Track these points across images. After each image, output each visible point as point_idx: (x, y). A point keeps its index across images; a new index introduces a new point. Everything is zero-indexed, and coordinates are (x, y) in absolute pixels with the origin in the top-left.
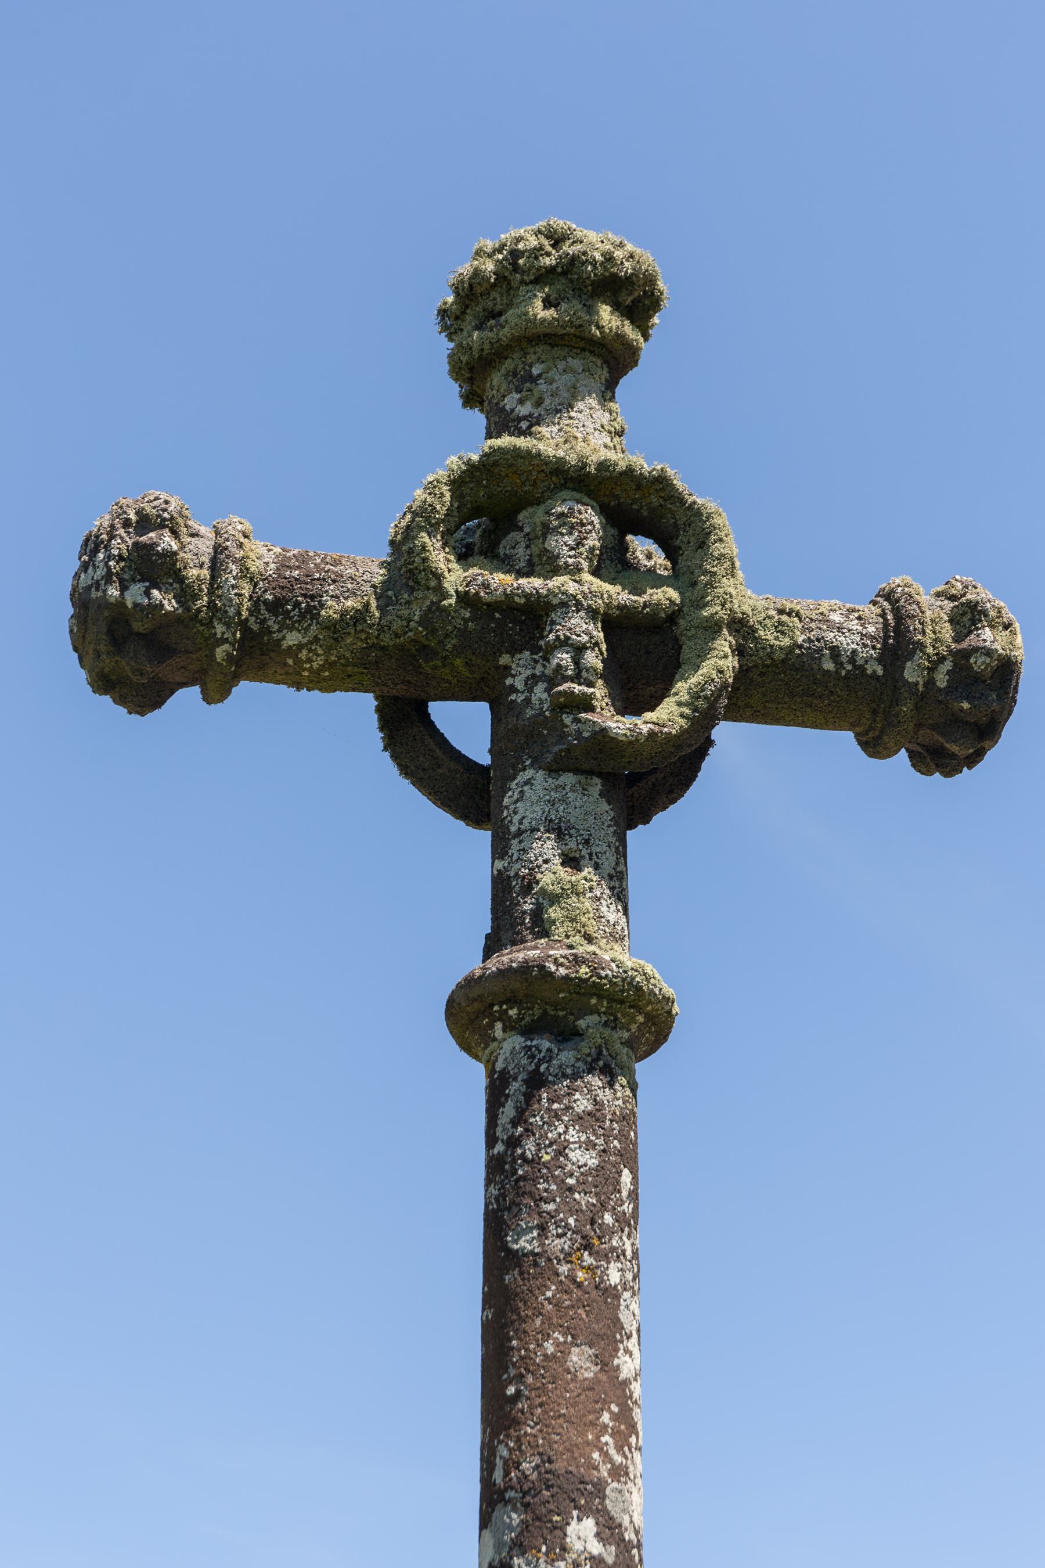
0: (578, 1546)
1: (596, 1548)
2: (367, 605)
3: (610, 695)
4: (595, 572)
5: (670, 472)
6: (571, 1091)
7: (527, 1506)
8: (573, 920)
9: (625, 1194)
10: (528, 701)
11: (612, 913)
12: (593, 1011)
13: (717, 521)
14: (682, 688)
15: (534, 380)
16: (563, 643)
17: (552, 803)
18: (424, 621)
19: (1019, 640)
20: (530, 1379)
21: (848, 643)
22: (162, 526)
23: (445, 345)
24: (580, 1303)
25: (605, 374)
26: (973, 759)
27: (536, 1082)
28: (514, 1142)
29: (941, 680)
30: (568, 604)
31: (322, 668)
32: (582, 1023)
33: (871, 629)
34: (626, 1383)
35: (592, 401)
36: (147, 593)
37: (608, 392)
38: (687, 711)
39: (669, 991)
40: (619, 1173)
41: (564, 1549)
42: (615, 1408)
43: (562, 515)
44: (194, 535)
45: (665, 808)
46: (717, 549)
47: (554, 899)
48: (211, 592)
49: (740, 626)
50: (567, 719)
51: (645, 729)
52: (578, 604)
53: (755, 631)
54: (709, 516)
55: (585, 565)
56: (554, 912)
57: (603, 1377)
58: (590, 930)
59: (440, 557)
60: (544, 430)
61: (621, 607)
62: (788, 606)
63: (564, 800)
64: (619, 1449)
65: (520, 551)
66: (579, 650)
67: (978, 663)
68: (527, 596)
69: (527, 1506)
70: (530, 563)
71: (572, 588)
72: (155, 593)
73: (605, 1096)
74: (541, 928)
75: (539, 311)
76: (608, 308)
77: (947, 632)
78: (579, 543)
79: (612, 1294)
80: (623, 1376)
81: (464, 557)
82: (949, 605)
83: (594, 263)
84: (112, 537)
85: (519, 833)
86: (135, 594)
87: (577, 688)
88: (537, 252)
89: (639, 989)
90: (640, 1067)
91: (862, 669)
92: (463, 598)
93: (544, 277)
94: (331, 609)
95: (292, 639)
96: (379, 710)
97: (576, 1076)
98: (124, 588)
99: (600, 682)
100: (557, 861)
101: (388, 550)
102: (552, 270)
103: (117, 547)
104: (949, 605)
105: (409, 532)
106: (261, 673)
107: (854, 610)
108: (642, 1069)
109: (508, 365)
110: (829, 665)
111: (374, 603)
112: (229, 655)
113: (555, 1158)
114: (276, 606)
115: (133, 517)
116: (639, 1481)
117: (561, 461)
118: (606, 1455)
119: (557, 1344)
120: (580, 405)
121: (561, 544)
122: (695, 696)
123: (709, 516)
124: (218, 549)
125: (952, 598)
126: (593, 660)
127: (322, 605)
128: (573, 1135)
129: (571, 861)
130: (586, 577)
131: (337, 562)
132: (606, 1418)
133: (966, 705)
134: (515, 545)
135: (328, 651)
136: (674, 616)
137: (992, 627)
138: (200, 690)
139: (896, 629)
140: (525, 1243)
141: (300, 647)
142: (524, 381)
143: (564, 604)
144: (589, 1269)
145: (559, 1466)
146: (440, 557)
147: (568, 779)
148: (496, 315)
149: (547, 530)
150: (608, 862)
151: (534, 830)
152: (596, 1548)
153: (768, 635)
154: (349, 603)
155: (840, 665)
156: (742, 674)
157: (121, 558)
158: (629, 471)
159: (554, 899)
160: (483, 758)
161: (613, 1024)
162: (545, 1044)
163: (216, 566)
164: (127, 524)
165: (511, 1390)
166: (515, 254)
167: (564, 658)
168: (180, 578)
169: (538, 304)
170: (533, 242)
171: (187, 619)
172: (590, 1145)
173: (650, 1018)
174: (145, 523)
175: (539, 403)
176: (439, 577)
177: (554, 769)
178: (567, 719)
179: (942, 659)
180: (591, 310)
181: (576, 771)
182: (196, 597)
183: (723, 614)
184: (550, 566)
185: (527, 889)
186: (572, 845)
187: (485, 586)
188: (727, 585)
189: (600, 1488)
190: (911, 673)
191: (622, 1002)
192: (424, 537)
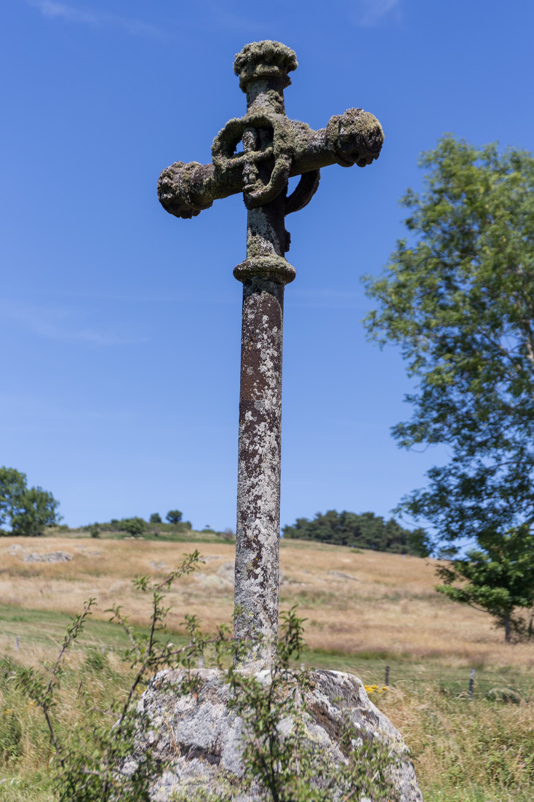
4: (256, 150)
12: (254, 276)
21: (317, 143)
24: (249, 356)
42: (258, 381)
52: (247, 163)
78: (247, 144)
79: (259, 350)
91: (322, 149)
110: (315, 152)
118: (255, 394)
120: (258, 97)
138: (336, 167)
141: (205, 193)
144: (252, 346)
152: (251, 418)
156: (292, 165)
172: (253, 313)
181: (255, 207)
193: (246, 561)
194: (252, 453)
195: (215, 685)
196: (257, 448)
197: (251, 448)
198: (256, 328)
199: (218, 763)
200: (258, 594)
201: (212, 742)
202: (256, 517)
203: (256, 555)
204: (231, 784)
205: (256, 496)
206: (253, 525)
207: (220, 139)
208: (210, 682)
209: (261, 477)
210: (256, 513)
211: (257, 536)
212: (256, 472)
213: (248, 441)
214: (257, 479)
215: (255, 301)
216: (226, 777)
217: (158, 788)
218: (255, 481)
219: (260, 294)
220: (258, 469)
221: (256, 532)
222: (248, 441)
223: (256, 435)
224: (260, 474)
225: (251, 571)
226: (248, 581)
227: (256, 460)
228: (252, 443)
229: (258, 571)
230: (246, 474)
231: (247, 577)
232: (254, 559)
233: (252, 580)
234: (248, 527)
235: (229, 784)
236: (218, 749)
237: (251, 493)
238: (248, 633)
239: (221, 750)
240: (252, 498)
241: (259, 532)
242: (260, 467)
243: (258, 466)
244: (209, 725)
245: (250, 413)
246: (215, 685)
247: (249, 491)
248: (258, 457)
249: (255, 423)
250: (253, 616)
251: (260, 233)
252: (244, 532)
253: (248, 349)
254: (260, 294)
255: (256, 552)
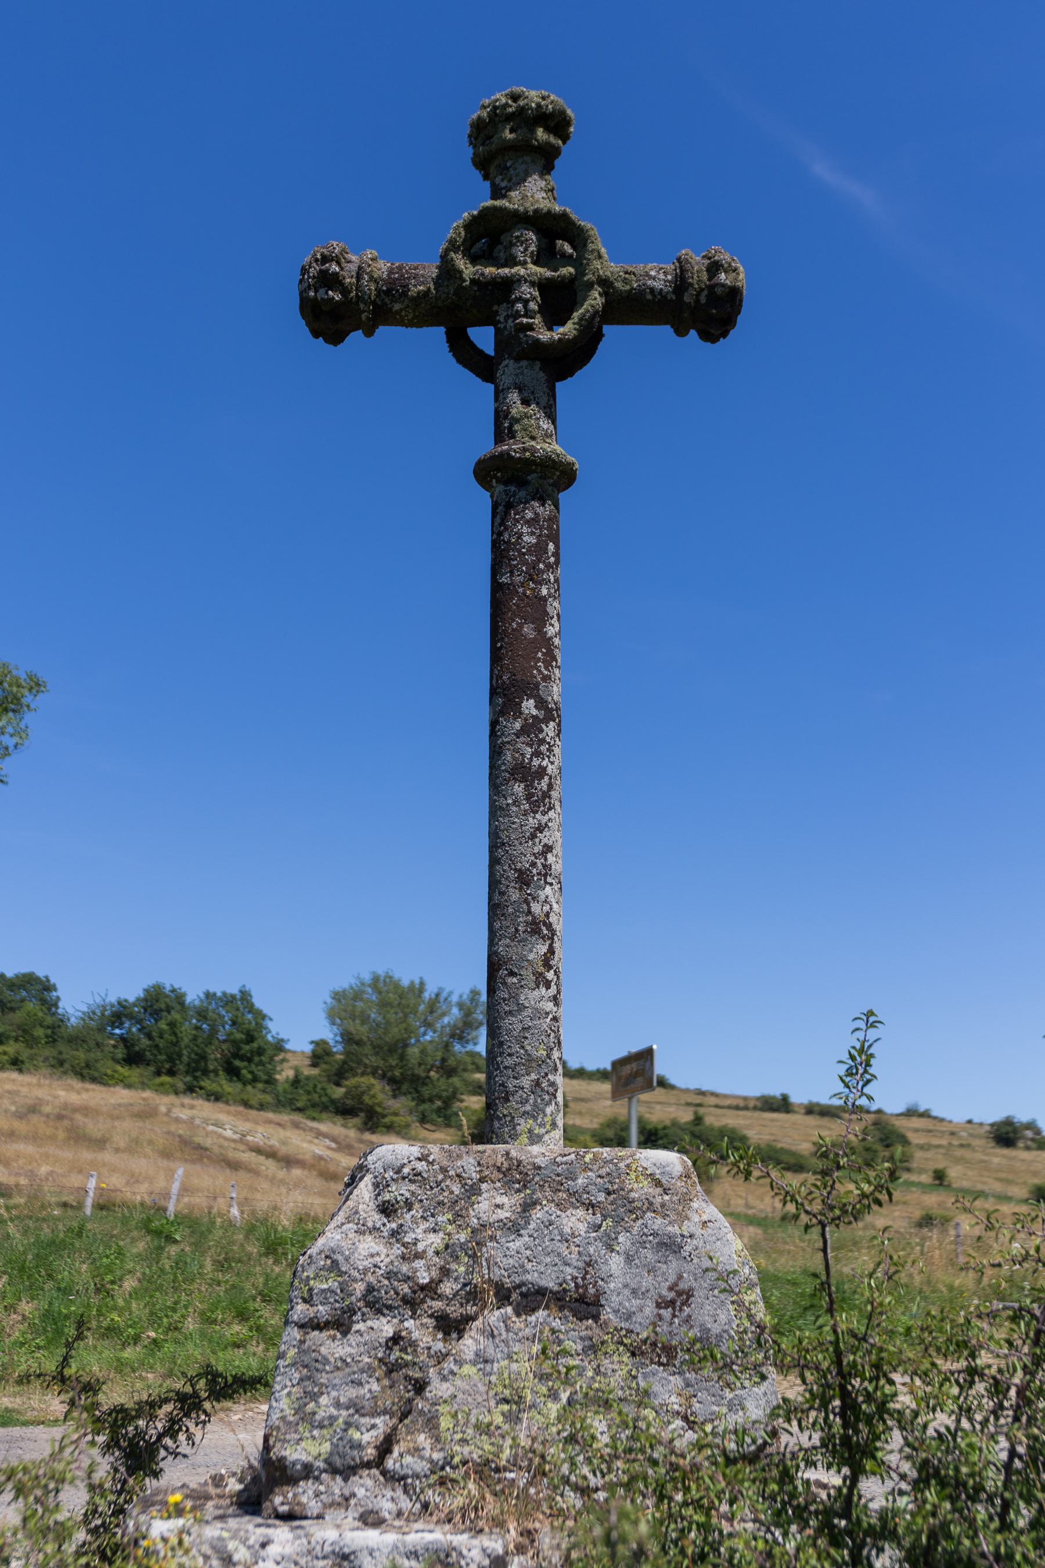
0: (527, 712)
1: (534, 712)
2: (429, 289)
3: (544, 321)
4: (536, 263)
5: (568, 210)
6: (525, 509)
7: (505, 695)
8: (525, 430)
9: (550, 554)
10: (505, 327)
11: (546, 425)
13: (591, 233)
14: (576, 315)
15: (507, 169)
16: (519, 299)
17: (517, 375)
18: (455, 294)
19: (742, 276)
20: (506, 640)
21: (658, 285)
22: (332, 260)
23: (470, 151)
24: (528, 605)
25: (543, 162)
26: (725, 334)
27: (509, 506)
28: (500, 534)
29: (703, 299)
30: (519, 280)
31: (413, 318)
32: (529, 478)
33: (669, 277)
34: (551, 638)
35: (536, 177)
36: (327, 293)
37: (547, 168)
38: (577, 327)
39: (570, 459)
40: (547, 545)
41: (521, 713)
42: (544, 650)
43: (517, 237)
44: (349, 262)
45: (581, 368)
46: (591, 246)
47: (517, 421)
48: (357, 289)
49: (605, 283)
50: (521, 335)
51: (556, 337)
52: (526, 281)
53: (612, 283)
54: (587, 231)
55: (529, 260)
56: (517, 427)
57: (538, 637)
58: (534, 434)
59: (461, 262)
60: (513, 194)
61: (547, 279)
62: (630, 269)
63: (522, 373)
64: (546, 668)
65: (502, 254)
66: (526, 302)
67: (719, 291)
68: (502, 278)
69: (505, 695)
70: (506, 260)
71: (522, 272)
72: (330, 292)
73: (540, 510)
74: (512, 435)
75: (508, 135)
76: (541, 129)
77: (705, 276)
78: (526, 250)
79: (544, 599)
80: (548, 636)
81: (474, 260)
82: (707, 262)
83: (532, 109)
84: (310, 267)
85: (503, 390)
86: (321, 294)
87: (525, 320)
88: (507, 105)
89: (553, 460)
90: (561, 496)
91: (665, 297)
92: (473, 281)
93: (510, 117)
94: (414, 290)
95: (397, 307)
96: (447, 333)
97: (526, 502)
98: (316, 292)
99: (538, 315)
100: (519, 402)
101: (439, 260)
102: (513, 113)
103: (313, 272)
104: (707, 262)
105: (446, 252)
106: (386, 323)
107: (661, 269)
108: (562, 496)
109: (497, 162)
110: (649, 297)
111: (432, 287)
112: (368, 317)
113: (517, 540)
114: (388, 293)
115: (319, 257)
116: (558, 681)
117: (516, 211)
118: (540, 672)
119: (518, 623)
120: (530, 179)
121: (519, 251)
122: (581, 319)
123: (587, 231)
124: (360, 268)
125: (709, 258)
126: (533, 306)
127: (409, 290)
128: (525, 530)
129: (526, 402)
130: (530, 266)
131: (416, 268)
132: (540, 655)
133: (714, 311)
134: (500, 253)
135: (414, 311)
136: (572, 280)
137: (726, 272)
139: (681, 277)
140: (504, 580)
141: (401, 310)
142: (504, 170)
143: (519, 281)
144: (533, 589)
145: (519, 677)
146: (461, 262)
147: (524, 363)
148: (490, 137)
149: (512, 245)
150: (544, 400)
151: (509, 388)
152: (534, 712)
153: (619, 285)
154: (421, 288)
155: (654, 296)
156: (605, 306)
157: (314, 277)
158: (549, 212)
159: (517, 421)
160: (491, 352)
161: (544, 477)
162: (513, 488)
163: (359, 277)
164: (317, 260)
165: (499, 645)
166: (495, 108)
167: (519, 306)
168: (341, 284)
169: (507, 131)
170: (504, 101)
171: (346, 302)
172: (532, 533)
173: (563, 472)
174: (325, 259)
175: (510, 180)
176: (461, 272)
177: (518, 359)
178: (521, 335)
179: (702, 290)
180: (533, 132)
181: (528, 359)
182: (350, 292)
183: (594, 279)
184: (512, 262)
185: (506, 417)
186: (526, 394)
187: (483, 274)
188: (597, 264)
189: (537, 686)
190: (687, 298)
191: (547, 466)
192: (452, 254)
193: (531, 957)
194: (536, 772)
195: (558, 1175)
196: (544, 763)
197: (536, 762)
198: (539, 561)
199: (596, 1318)
200: (551, 1016)
201: (574, 1279)
202: (546, 883)
203: (547, 947)
204: (633, 1354)
205: (545, 845)
206: (542, 895)
207: (468, 227)
208: (545, 1168)
209: (551, 814)
210: (545, 875)
211: (547, 915)
212: (544, 806)
213: (528, 751)
214: (546, 817)
215: (536, 514)
216: (621, 1343)
217: (455, 1369)
218: (544, 819)
219: (543, 505)
220: (547, 800)
221: (546, 908)
222: (528, 751)
223: (542, 741)
224: (550, 809)
225: (541, 974)
226: (536, 993)
227: (544, 784)
228: (537, 754)
229: (550, 976)
230: (527, 807)
231: (533, 985)
232: (545, 954)
233: (543, 990)
234: (534, 899)
235: (628, 1355)
236: (592, 1290)
237: (537, 840)
238: (538, 1083)
239: (598, 1295)
240: (538, 849)
241: (551, 909)
242: (550, 797)
243: (546, 795)
244: (563, 1248)
245: (532, 701)
246: (558, 1175)
247: (533, 836)
248: (546, 778)
249: (541, 721)
250: (545, 1053)
251: (537, 404)
252: (525, 907)
253: (524, 594)
254: (543, 505)
255: (548, 942)
